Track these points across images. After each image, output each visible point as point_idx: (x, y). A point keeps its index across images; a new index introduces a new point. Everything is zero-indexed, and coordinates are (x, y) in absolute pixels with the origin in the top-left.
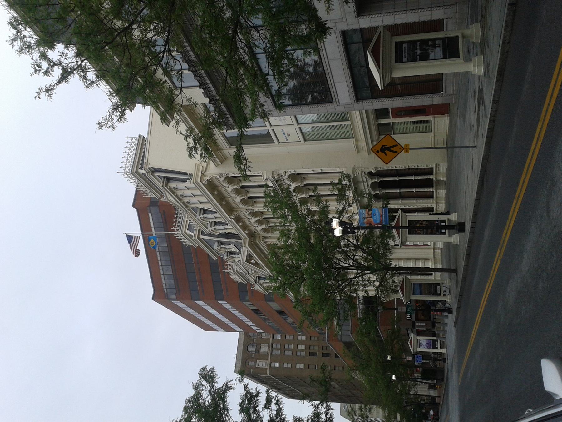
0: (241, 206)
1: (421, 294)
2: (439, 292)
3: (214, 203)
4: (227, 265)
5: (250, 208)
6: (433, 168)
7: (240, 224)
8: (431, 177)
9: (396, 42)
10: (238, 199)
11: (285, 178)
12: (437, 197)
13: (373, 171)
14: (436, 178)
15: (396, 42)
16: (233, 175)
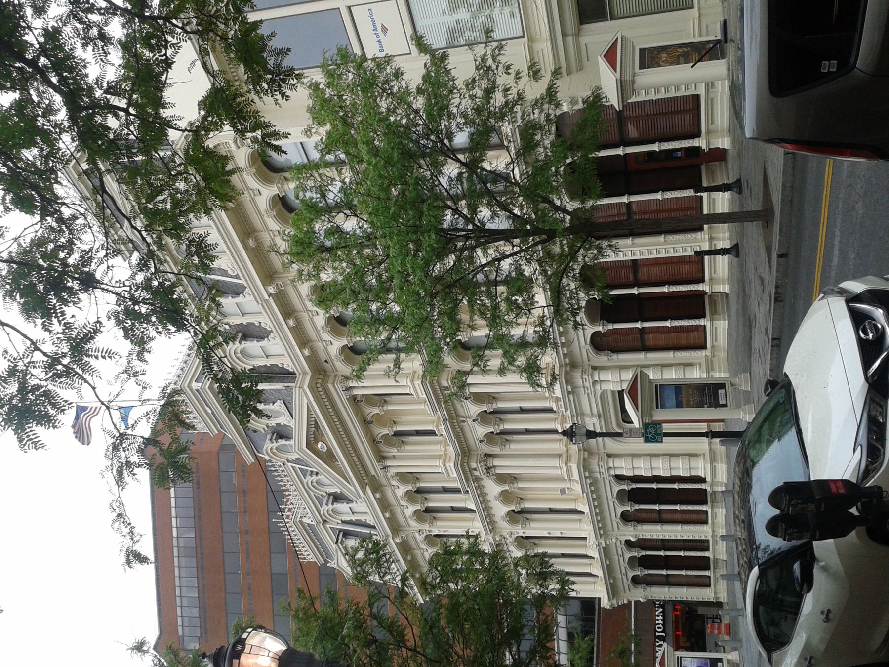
0: (413, 523)
1: (679, 405)
2: (722, 402)
3: (289, 343)
4: (286, 503)
5: (426, 527)
6: (697, 97)
7: (378, 495)
8: (700, 287)
9: (640, 50)
10: (410, 510)
11: (508, 542)
12: (713, 347)
13: (632, 539)
14: (711, 288)
15: (640, 50)
16: (437, 532)
